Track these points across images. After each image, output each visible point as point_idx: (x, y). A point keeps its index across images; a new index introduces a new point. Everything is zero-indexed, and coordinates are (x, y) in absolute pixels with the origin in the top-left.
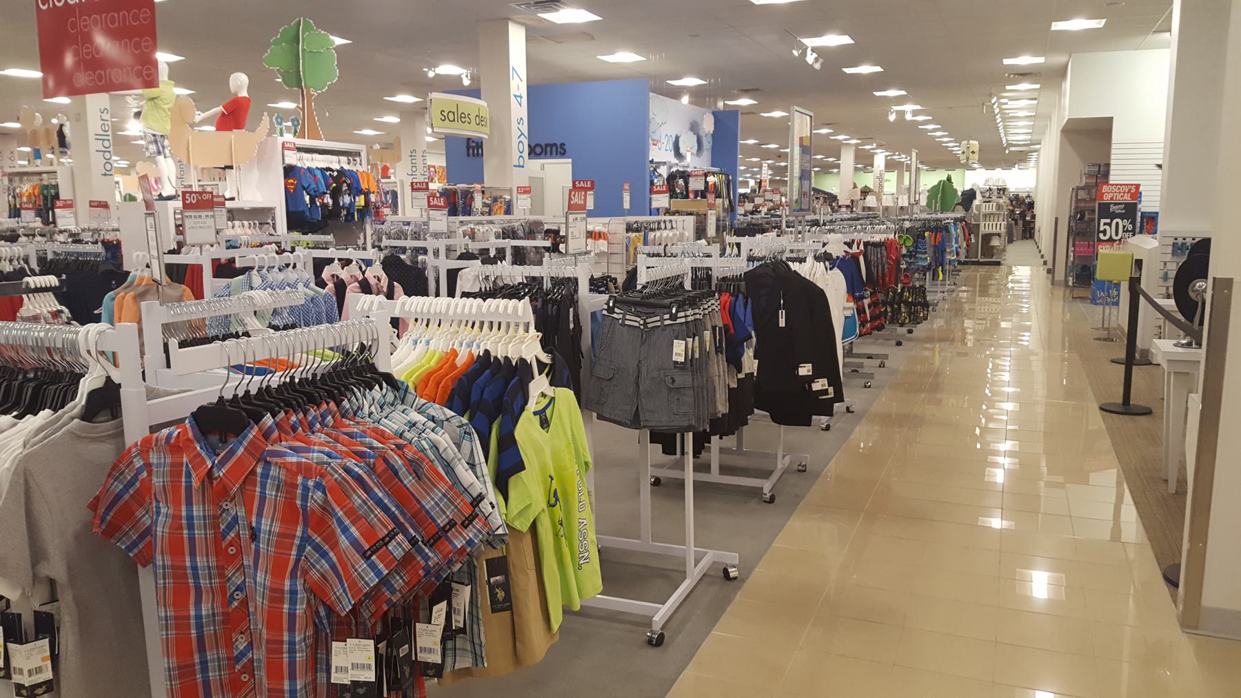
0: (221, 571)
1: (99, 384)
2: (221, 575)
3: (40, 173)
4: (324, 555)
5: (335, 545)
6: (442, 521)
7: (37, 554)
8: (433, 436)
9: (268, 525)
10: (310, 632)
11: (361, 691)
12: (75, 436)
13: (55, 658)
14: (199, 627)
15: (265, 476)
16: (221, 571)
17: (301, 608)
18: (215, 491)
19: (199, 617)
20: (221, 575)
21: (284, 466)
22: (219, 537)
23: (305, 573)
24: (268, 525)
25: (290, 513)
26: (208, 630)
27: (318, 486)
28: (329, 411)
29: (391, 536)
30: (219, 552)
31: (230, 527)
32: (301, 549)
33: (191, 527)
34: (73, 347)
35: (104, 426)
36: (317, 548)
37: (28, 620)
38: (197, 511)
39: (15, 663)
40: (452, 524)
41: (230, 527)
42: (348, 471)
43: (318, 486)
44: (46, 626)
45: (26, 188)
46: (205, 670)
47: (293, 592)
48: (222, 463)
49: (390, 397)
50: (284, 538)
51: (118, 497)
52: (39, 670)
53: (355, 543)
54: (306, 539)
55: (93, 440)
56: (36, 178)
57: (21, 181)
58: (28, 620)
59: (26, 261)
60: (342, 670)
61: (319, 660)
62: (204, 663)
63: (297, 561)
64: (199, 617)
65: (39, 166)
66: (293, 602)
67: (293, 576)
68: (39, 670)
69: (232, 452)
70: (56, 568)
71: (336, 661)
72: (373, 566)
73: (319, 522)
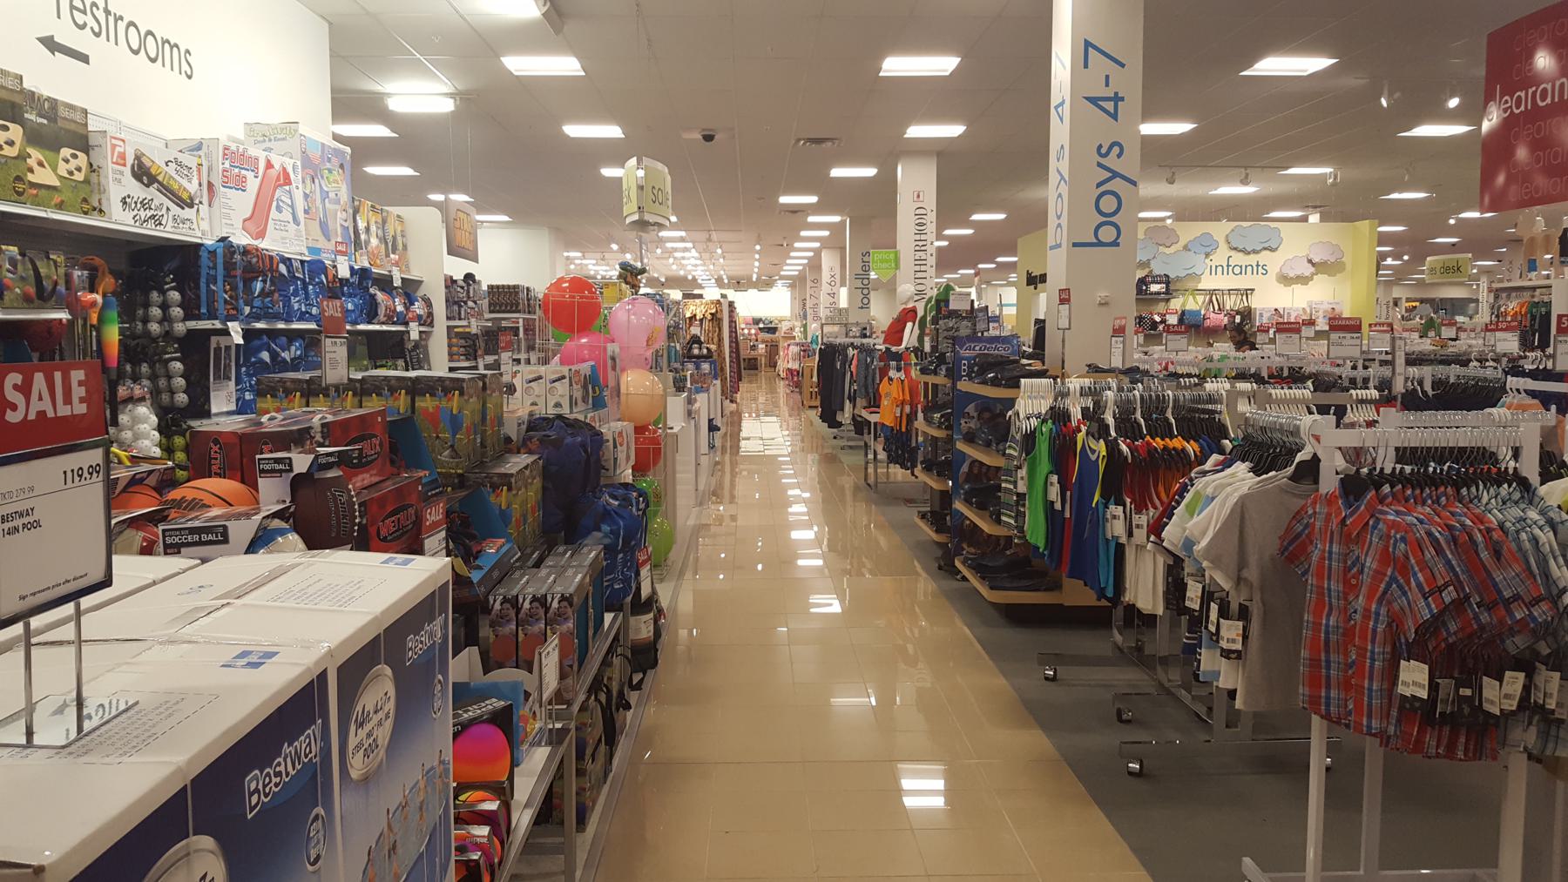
0: (1346, 595)
1: (1308, 457)
2: (1346, 599)
3: (1534, 288)
4: (1405, 593)
5: (1408, 583)
6: (1507, 594)
7: (1242, 564)
8: (1537, 531)
9: (1370, 563)
10: (1388, 649)
11: (1417, 704)
12: (1282, 489)
13: (1245, 637)
14: (1327, 633)
15: (1375, 527)
16: (1346, 595)
17: (1381, 628)
18: (1347, 539)
19: (1327, 626)
20: (1346, 599)
21: (1385, 521)
22: (1347, 570)
23: (1389, 603)
24: (1370, 563)
25: (1386, 557)
26: (1333, 638)
27: (1403, 539)
28: (1445, 494)
29: (1446, 585)
30: (1346, 582)
31: (1354, 564)
32: (1389, 585)
33: (1330, 559)
34: (1295, 432)
35: (1305, 487)
36: (1400, 587)
37: (1234, 607)
38: (1335, 549)
39: (1223, 633)
40: (1517, 597)
41: (1354, 564)
42: (1429, 534)
43: (1403, 539)
44: (1244, 614)
45: (1512, 306)
46: (1328, 667)
47: (1377, 614)
48: (1352, 514)
49: (1517, 495)
50: (1379, 574)
51: (1300, 534)
52: (1234, 641)
53: (1419, 585)
54: (1393, 579)
55: (1295, 495)
56: (1527, 294)
57: (1508, 297)
58: (1234, 607)
59: (1421, 383)
60: (1405, 684)
61: (1392, 675)
62: (1328, 662)
63: (1385, 593)
64: (1327, 626)
65: (1534, 279)
66: (1376, 621)
67: (1380, 602)
68: (1234, 641)
69: (1358, 508)
70: (1252, 574)
71: (1403, 676)
72: (1428, 605)
73: (1404, 569)
